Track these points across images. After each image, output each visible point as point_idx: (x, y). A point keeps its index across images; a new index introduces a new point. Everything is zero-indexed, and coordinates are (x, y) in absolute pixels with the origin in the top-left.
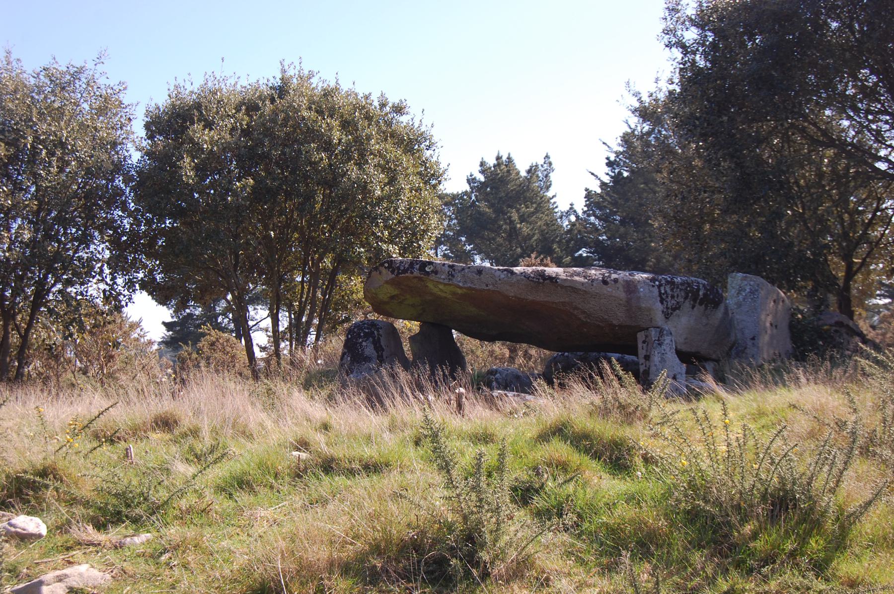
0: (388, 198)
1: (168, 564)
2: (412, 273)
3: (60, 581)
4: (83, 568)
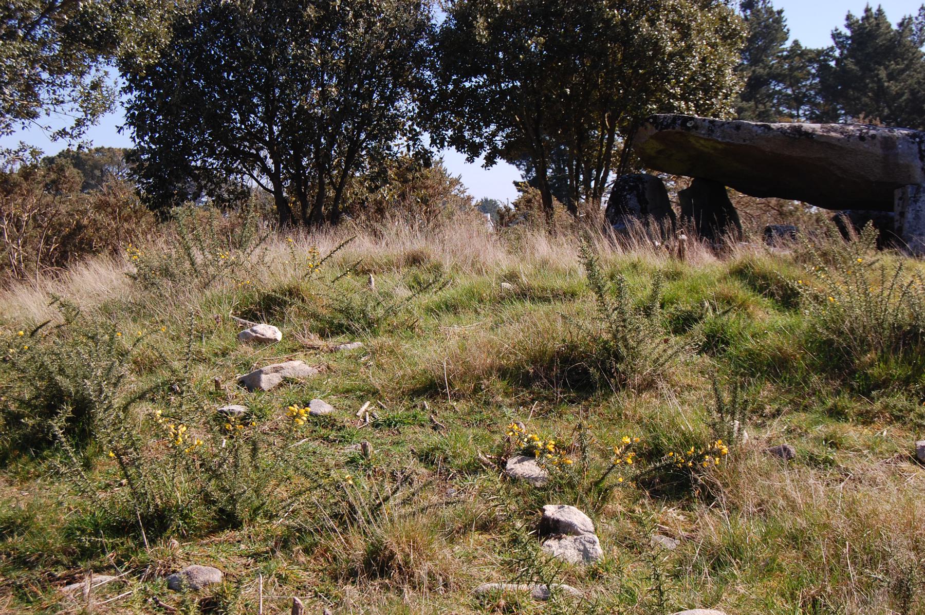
0: (680, 54)
1: (365, 364)
2: (674, 128)
3: (277, 371)
4: (296, 363)
